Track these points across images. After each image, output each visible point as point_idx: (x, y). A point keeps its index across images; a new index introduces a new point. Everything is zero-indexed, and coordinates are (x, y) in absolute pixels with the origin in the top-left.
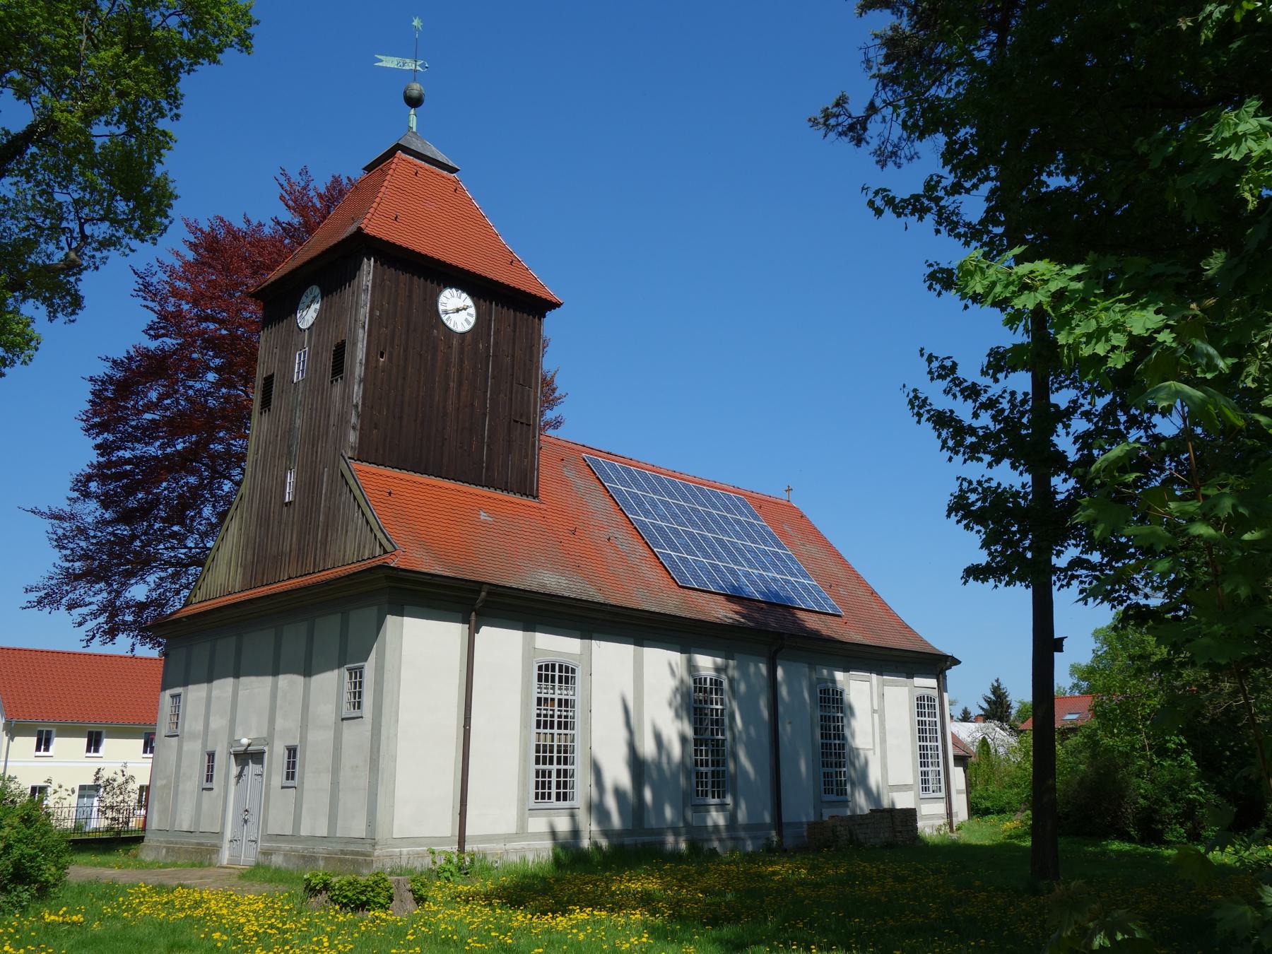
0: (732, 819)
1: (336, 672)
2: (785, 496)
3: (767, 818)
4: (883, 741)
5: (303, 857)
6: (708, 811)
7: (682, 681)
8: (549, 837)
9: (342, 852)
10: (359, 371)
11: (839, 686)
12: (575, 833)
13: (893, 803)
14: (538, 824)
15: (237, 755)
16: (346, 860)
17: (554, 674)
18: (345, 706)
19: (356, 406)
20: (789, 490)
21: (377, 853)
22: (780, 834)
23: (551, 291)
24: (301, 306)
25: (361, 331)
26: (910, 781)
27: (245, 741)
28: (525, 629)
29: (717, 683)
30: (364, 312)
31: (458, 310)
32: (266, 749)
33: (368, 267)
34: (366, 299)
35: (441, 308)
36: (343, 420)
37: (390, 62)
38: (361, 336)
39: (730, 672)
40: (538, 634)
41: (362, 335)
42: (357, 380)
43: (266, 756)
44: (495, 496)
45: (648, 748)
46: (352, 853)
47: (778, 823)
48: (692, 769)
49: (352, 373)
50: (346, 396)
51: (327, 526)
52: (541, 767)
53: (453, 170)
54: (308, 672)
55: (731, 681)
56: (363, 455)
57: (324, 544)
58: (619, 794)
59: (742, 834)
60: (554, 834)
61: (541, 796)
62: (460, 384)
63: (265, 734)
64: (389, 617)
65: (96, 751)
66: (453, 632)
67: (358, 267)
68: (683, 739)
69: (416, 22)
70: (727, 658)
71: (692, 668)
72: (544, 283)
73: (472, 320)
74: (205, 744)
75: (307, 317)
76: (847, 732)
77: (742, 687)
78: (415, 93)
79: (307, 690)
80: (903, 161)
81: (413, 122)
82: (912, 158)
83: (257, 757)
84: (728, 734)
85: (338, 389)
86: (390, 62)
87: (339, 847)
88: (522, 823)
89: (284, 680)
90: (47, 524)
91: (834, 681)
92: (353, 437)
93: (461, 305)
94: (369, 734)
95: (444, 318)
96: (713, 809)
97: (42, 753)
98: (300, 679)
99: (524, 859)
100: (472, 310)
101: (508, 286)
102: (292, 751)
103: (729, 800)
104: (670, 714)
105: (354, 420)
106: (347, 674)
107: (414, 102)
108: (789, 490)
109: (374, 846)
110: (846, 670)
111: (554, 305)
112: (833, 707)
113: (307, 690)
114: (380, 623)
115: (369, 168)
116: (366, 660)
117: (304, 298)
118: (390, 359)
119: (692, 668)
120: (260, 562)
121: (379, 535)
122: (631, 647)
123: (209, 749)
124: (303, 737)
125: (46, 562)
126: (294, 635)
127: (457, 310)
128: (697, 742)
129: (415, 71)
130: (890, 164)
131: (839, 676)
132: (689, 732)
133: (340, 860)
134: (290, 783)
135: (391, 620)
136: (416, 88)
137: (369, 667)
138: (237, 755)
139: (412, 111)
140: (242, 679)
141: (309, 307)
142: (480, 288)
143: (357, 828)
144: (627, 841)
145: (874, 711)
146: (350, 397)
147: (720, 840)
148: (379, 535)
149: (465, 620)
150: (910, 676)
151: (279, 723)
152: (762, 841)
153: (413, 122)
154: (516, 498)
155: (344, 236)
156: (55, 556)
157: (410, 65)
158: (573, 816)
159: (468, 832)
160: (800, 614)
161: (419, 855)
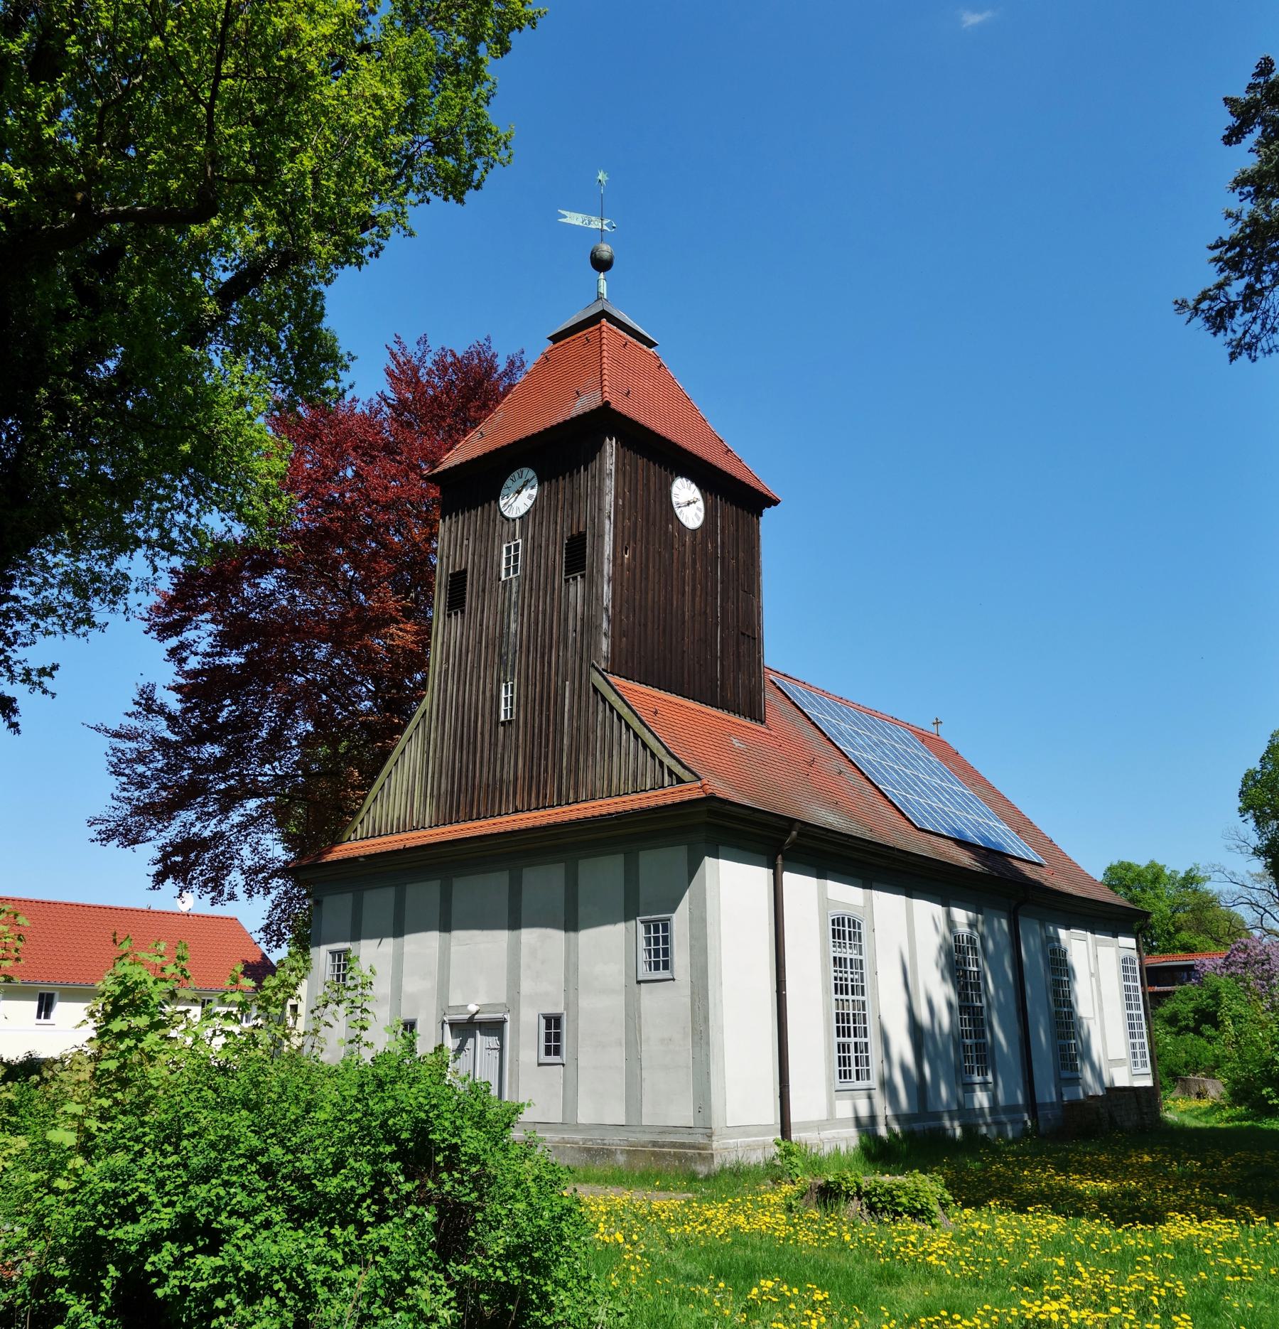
0: (993, 1099)
1: (621, 926)
2: (933, 729)
3: (1020, 1099)
4: (1101, 1009)
5: (588, 1150)
6: (974, 1091)
7: (945, 939)
8: (852, 1123)
9: (655, 1144)
10: (607, 568)
11: (1063, 944)
12: (873, 1118)
13: (1112, 1081)
14: (844, 1110)
15: (453, 1025)
16: (664, 1154)
17: (844, 930)
18: (643, 968)
19: (607, 610)
20: (937, 723)
21: (715, 1145)
22: (1034, 1116)
23: (769, 485)
24: (504, 491)
25: (607, 522)
26: (1124, 1056)
27: (473, 1008)
28: (819, 876)
29: (971, 940)
30: (609, 499)
31: (689, 504)
32: (507, 1017)
33: (610, 446)
34: (610, 484)
35: (674, 500)
36: (589, 627)
37: (575, 219)
38: (607, 527)
39: (980, 927)
40: (829, 882)
41: (608, 527)
42: (606, 579)
43: (508, 1026)
44: (724, 717)
45: (924, 1016)
46: (673, 1145)
47: (1032, 1104)
48: (957, 1038)
49: (601, 571)
50: (591, 597)
51: (575, 750)
52: (842, 1039)
53: (651, 344)
54: (571, 924)
55: (982, 937)
56: (623, 665)
57: (574, 770)
58: (904, 1070)
59: (1003, 1118)
60: (857, 1120)
61: (844, 1075)
62: (694, 589)
63: (503, 999)
64: (706, 858)
65: (47, 1017)
66: (759, 876)
67: (599, 447)
68: (950, 1005)
69: (601, 176)
70: (977, 912)
71: (951, 923)
72: (766, 478)
73: (701, 515)
74: (396, 1009)
75: (518, 502)
76: (1073, 999)
77: (990, 945)
78: (606, 255)
79: (514, 950)
80: (1259, 354)
81: (603, 288)
82: (1270, 351)
83: (495, 1028)
84: (984, 1000)
85: (577, 589)
86: (575, 219)
87: (647, 1138)
88: (831, 1109)
89: (529, 936)
90: (105, 743)
91: (1058, 940)
92: (605, 645)
93: (691, 498)
94: (688, 1000)
95: (678, 511)
96: (977, 1087)
97: (42, 1021)
98: (558, 936)
99: (837, 1150)
100: (701, 504)
101: (734, 478)
102: (553, 1022)
103: (990, 1078)
104: (937, 975)
105: (605, 625)
106: (641, 928)
107: (601, 265)
108: (937, 723)
109: (710, 1136)
110: (1068, 928)
111: (775, 502)
112: (1059, 966)
113: (514, 950)
114: (693, 867)
115: (555, 339)
116: (673, 910)
117: (508, 482)
118: (634, 556)
119: (951, 923)
120: (460, 796)
121: (668, 761)
122: (901, 899)
123: (407, 1015)
124: (572, 1003)
125: (103, 794)
126: (543, 881)
127: (689, 505)
128: (963, 1009)
129: (602, 230)
130: (1244, 358)
131: (1062, 933)
132: (954, 999)
133: (654, 1153)
134: (552, 1059)
135: (708, 861)
136: (605, 250)
137: (680, 920)
138: (453, 1025)
139: (602, 275)
140: (456, 934)
141: (519, 492)
142: (713, 481)
143: (679, 1114)
144: (916, 1126)
145: (1092, 975)
146: (599, 598)
147: (987, 1125)
148: (668, 761)
149: (771, 865)
150: (1115, 936)
151: (526, 986)
152: (1020, 1126)
153: (603, 288)
154: (747, 722)
155: (574, 413)
156: (113, 783)
157: (596, 224)
158: (870, 1097)
159: (795, 1117)
160: (1016, 863)
161: (751, 1148)
